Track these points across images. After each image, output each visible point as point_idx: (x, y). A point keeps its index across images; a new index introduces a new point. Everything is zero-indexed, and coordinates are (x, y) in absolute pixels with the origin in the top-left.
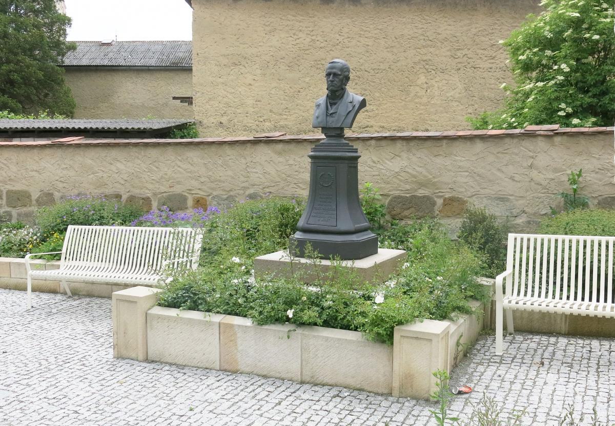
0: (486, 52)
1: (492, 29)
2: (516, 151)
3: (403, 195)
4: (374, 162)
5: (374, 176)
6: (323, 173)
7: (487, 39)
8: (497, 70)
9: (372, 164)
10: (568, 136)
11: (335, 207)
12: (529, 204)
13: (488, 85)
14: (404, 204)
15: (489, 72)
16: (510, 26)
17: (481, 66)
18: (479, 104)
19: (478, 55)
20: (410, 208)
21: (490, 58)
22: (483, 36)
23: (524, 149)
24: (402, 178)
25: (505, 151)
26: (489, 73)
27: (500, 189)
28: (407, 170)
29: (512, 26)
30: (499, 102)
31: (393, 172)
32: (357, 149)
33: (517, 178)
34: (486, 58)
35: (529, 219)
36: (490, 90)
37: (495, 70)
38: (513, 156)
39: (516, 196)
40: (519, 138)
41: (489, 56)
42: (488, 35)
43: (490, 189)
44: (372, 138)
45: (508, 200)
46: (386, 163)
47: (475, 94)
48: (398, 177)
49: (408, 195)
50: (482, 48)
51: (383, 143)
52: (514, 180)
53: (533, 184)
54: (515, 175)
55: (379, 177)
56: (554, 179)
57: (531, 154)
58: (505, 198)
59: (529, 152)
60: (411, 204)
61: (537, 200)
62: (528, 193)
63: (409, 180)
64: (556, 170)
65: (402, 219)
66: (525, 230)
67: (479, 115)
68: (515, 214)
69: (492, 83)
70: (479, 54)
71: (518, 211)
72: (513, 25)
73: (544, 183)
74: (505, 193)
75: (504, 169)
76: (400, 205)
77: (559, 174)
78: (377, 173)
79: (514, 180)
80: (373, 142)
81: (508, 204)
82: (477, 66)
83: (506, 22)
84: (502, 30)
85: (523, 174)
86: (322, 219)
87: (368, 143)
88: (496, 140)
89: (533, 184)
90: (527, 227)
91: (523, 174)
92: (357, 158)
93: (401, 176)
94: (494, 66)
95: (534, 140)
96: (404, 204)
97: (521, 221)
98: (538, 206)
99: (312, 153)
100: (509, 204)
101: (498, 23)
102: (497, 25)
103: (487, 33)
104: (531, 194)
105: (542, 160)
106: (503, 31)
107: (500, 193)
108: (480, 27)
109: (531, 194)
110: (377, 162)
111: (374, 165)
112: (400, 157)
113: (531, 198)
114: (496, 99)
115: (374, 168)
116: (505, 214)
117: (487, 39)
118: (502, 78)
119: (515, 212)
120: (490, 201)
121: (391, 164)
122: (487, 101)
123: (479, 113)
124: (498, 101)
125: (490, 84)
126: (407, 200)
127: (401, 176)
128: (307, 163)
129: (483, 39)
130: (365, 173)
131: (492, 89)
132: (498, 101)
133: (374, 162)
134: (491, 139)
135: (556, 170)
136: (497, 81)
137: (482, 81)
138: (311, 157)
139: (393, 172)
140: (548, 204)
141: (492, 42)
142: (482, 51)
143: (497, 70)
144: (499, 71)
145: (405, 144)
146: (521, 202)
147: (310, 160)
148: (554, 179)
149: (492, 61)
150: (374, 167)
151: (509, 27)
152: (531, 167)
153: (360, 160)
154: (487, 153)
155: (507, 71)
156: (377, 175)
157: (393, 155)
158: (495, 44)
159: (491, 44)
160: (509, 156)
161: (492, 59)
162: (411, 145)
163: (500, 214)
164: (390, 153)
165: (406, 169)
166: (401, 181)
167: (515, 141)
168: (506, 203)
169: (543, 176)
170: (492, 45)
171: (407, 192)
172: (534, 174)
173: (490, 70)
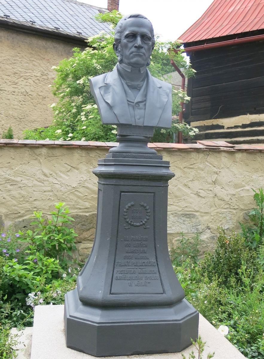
0: (9, 78)
1: (15, 60)
2: (201, 166)
3: (81, 214)
4: (45, 175)
5: (45, 192)
6: (132, 203)
7: (11, 68)
8: (19, 94)
9: (43, 177)
10: (247, 153)
11: (153, 260)
12: (213, 219)
13: (12, 105)
14: (83, 225)
15: (13, 95)
16: (28, 59)
17: (6, 89)
18: (5, 121)
19: (3, 79)
20: (91, 228)
21: (14, 83)
22: (8, 65)
23: (209, 165)
24: (80, 194)
25: (191, 166)
26: (13, 96)
27: (187, 205)
28: (87, 184)
29: (30, 60)
30: (21, 120)
31: (70, 188)
32: (168, 163)
33: (202, 193)
34: (10, 83)
35: (213, 235)
36: (14, 110)
37: (17, 94)
38: (199, 171)
39: (201, 212)
40: (205, 153)
41: (13, 81)
42: (11, 64)
43: (176, 205)
44: (44, 146)
45: (194, 216)
46: (61, 177)
47: (2, 112)
48: (76, 193)
49: (87, 214)
50: (7, 74)
51: (57, 152)
52: (199, 196)
53: (216, 199)
54: (201, 191)
55: (51, 194)
56: (235, 195)
57: (215, 170)
58: (193, 214)
59: (214, 168)
60: (92, 225)
61: (221, 215)
62: (212, 209)
63: (89, 197)
64: (236, 186)
65: (81, 242)
66: (209, 246)
67: (6, 129)
68: (201, 231)
69: (15, 104)
70: (5, 79)
71: (203, 227)
72: (31, 59)
73: (227, 198)
74: (190, 210)
75: (190, 184)
76: (78, 226)
77: (239, 190)
78: (49, 188)
79: (199, 196)
80: (44, 151)
81: (194, 220)
82: (3, 89)
83: (25, 56)
84: (21, 62)
85: (208, 190)
86: (136, 282)
87: (38, 151)
88: (183, 155)
89: (216, 199)
90: (211, 243)
91: (208, 190)
92: (166, 179)
93: (80, 192)
94: (16, 90)
95: (217, 155)
96: (83, 225)
97: (205, 237)
98: (221, 221)
99: (104, 169)
100: (195, 220)
101: (19, 55)
102: (18, 57)
103: (11, 62)
104: (214, 210)
105: (225, 176)
106: (23, 63)
107: (186, 209)
108: (5, 57)
109: (214, 210)
110: (49, 175)
111: (46, 178)
112: (77, 169)
113: (215, 214)
114: (19, 118)
115: (45, 182)
116: (191, 231)
117: (11, 68)
118: (23, 101)
119: (201, 228)
120: (176, 218)
121: (67, 178)
122: (12, 119)
123: (5, 128)
124: (21, 119)
125: (14, 105)
126: (87, 219)
127: (80, 192)
128: (94, 183)
129: (7, 66)
130: (33, 189)
131: (16, 109)
132: (21, 119)
133: (45, 175)
134: (178, 153)
135: (236, 186)
136: (19, 103)
137: (7, 102)
138: (100, 176)
139: (70, 188)
140: (230, 220)
141: (15, 70)
142: (6, 77)
143: (19, 94)
144: (21, 95)
145: (84, 155)
146: (206, 218)
147: (96, 179)
148: (235, 195)
149: (15, 86)
150: (46, 181)
151: (27, 60)
152: (214, 183)
153: (171, 183)
154: (174, 167)
155: (27, 96)
156: (49, 191)
157: (70, 167)
158: (17, 72)
159: (13, 72)
160: (195, 172)
161: (15, 84)
162: (91, 155)
163: (186, 231)
164: (66, 165)
165: (86, 183)
166: (79, 197)
167: (201, 155)
168: (192, 219)
169: (226, 192)
170: (15, 73)
171: (86, 210)
172: (217, 189)
173: (14, 93)
